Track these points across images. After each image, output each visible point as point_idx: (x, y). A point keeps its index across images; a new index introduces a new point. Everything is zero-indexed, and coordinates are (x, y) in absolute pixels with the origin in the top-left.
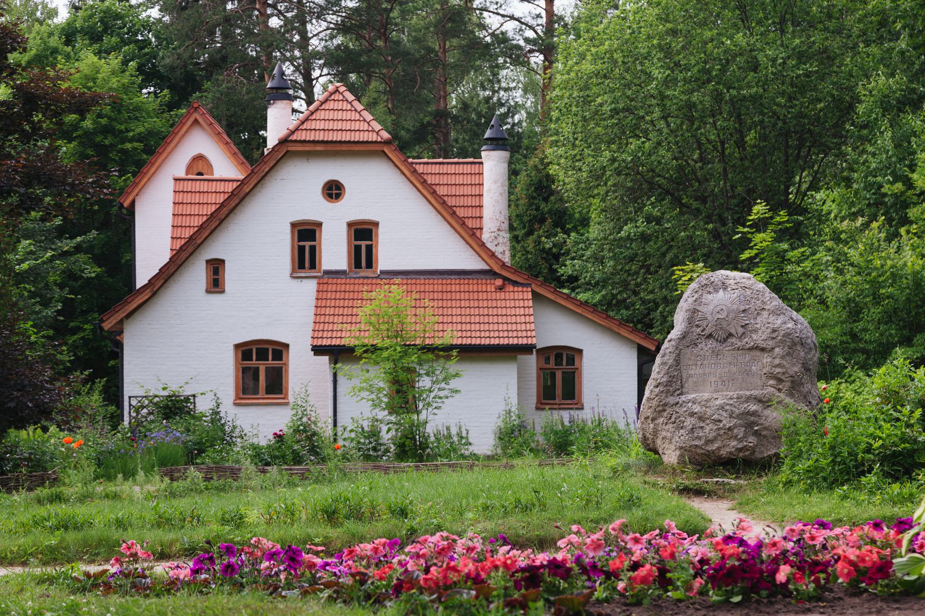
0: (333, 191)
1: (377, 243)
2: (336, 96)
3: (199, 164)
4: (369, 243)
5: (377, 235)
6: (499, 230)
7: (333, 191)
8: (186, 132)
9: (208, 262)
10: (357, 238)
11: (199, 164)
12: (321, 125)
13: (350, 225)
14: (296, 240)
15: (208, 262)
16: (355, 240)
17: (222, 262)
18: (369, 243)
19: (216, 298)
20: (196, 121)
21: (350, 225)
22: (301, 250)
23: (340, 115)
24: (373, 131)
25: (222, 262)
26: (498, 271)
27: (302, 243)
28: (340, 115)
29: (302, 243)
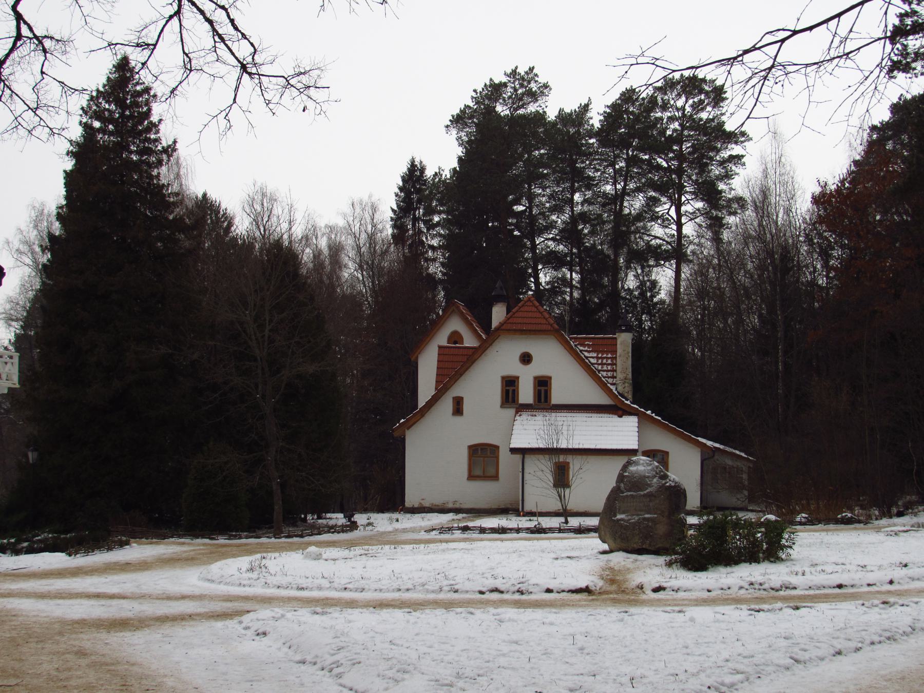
0: (526, 359)
1: (551, 388)
2: (528, 303)
3: (455, 337)
4: (546, 388)
5: (551, 384)
6: (625, 379)
7: (526, 359)
8: (450, 315)
9: (454, 398)
10: (507, 386)
11: (455, 337)
12: (520, 320)
13: (503, 378)
14: (504, 386)
15: (454, 398)
16: (538, 386)
17: (462, 398)
18: (546, 388)
19: (458, 419)
20: (454, 310)
21: (503, 378)
22: (507, 392)
23: (530, 315)
24: (549, 324)
25: (462, 398)
26: (619, 406)
27: (507, 388)
28: (530, 315)
29: (507, 388)
